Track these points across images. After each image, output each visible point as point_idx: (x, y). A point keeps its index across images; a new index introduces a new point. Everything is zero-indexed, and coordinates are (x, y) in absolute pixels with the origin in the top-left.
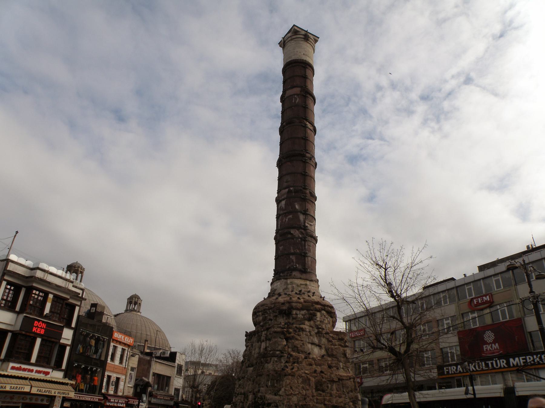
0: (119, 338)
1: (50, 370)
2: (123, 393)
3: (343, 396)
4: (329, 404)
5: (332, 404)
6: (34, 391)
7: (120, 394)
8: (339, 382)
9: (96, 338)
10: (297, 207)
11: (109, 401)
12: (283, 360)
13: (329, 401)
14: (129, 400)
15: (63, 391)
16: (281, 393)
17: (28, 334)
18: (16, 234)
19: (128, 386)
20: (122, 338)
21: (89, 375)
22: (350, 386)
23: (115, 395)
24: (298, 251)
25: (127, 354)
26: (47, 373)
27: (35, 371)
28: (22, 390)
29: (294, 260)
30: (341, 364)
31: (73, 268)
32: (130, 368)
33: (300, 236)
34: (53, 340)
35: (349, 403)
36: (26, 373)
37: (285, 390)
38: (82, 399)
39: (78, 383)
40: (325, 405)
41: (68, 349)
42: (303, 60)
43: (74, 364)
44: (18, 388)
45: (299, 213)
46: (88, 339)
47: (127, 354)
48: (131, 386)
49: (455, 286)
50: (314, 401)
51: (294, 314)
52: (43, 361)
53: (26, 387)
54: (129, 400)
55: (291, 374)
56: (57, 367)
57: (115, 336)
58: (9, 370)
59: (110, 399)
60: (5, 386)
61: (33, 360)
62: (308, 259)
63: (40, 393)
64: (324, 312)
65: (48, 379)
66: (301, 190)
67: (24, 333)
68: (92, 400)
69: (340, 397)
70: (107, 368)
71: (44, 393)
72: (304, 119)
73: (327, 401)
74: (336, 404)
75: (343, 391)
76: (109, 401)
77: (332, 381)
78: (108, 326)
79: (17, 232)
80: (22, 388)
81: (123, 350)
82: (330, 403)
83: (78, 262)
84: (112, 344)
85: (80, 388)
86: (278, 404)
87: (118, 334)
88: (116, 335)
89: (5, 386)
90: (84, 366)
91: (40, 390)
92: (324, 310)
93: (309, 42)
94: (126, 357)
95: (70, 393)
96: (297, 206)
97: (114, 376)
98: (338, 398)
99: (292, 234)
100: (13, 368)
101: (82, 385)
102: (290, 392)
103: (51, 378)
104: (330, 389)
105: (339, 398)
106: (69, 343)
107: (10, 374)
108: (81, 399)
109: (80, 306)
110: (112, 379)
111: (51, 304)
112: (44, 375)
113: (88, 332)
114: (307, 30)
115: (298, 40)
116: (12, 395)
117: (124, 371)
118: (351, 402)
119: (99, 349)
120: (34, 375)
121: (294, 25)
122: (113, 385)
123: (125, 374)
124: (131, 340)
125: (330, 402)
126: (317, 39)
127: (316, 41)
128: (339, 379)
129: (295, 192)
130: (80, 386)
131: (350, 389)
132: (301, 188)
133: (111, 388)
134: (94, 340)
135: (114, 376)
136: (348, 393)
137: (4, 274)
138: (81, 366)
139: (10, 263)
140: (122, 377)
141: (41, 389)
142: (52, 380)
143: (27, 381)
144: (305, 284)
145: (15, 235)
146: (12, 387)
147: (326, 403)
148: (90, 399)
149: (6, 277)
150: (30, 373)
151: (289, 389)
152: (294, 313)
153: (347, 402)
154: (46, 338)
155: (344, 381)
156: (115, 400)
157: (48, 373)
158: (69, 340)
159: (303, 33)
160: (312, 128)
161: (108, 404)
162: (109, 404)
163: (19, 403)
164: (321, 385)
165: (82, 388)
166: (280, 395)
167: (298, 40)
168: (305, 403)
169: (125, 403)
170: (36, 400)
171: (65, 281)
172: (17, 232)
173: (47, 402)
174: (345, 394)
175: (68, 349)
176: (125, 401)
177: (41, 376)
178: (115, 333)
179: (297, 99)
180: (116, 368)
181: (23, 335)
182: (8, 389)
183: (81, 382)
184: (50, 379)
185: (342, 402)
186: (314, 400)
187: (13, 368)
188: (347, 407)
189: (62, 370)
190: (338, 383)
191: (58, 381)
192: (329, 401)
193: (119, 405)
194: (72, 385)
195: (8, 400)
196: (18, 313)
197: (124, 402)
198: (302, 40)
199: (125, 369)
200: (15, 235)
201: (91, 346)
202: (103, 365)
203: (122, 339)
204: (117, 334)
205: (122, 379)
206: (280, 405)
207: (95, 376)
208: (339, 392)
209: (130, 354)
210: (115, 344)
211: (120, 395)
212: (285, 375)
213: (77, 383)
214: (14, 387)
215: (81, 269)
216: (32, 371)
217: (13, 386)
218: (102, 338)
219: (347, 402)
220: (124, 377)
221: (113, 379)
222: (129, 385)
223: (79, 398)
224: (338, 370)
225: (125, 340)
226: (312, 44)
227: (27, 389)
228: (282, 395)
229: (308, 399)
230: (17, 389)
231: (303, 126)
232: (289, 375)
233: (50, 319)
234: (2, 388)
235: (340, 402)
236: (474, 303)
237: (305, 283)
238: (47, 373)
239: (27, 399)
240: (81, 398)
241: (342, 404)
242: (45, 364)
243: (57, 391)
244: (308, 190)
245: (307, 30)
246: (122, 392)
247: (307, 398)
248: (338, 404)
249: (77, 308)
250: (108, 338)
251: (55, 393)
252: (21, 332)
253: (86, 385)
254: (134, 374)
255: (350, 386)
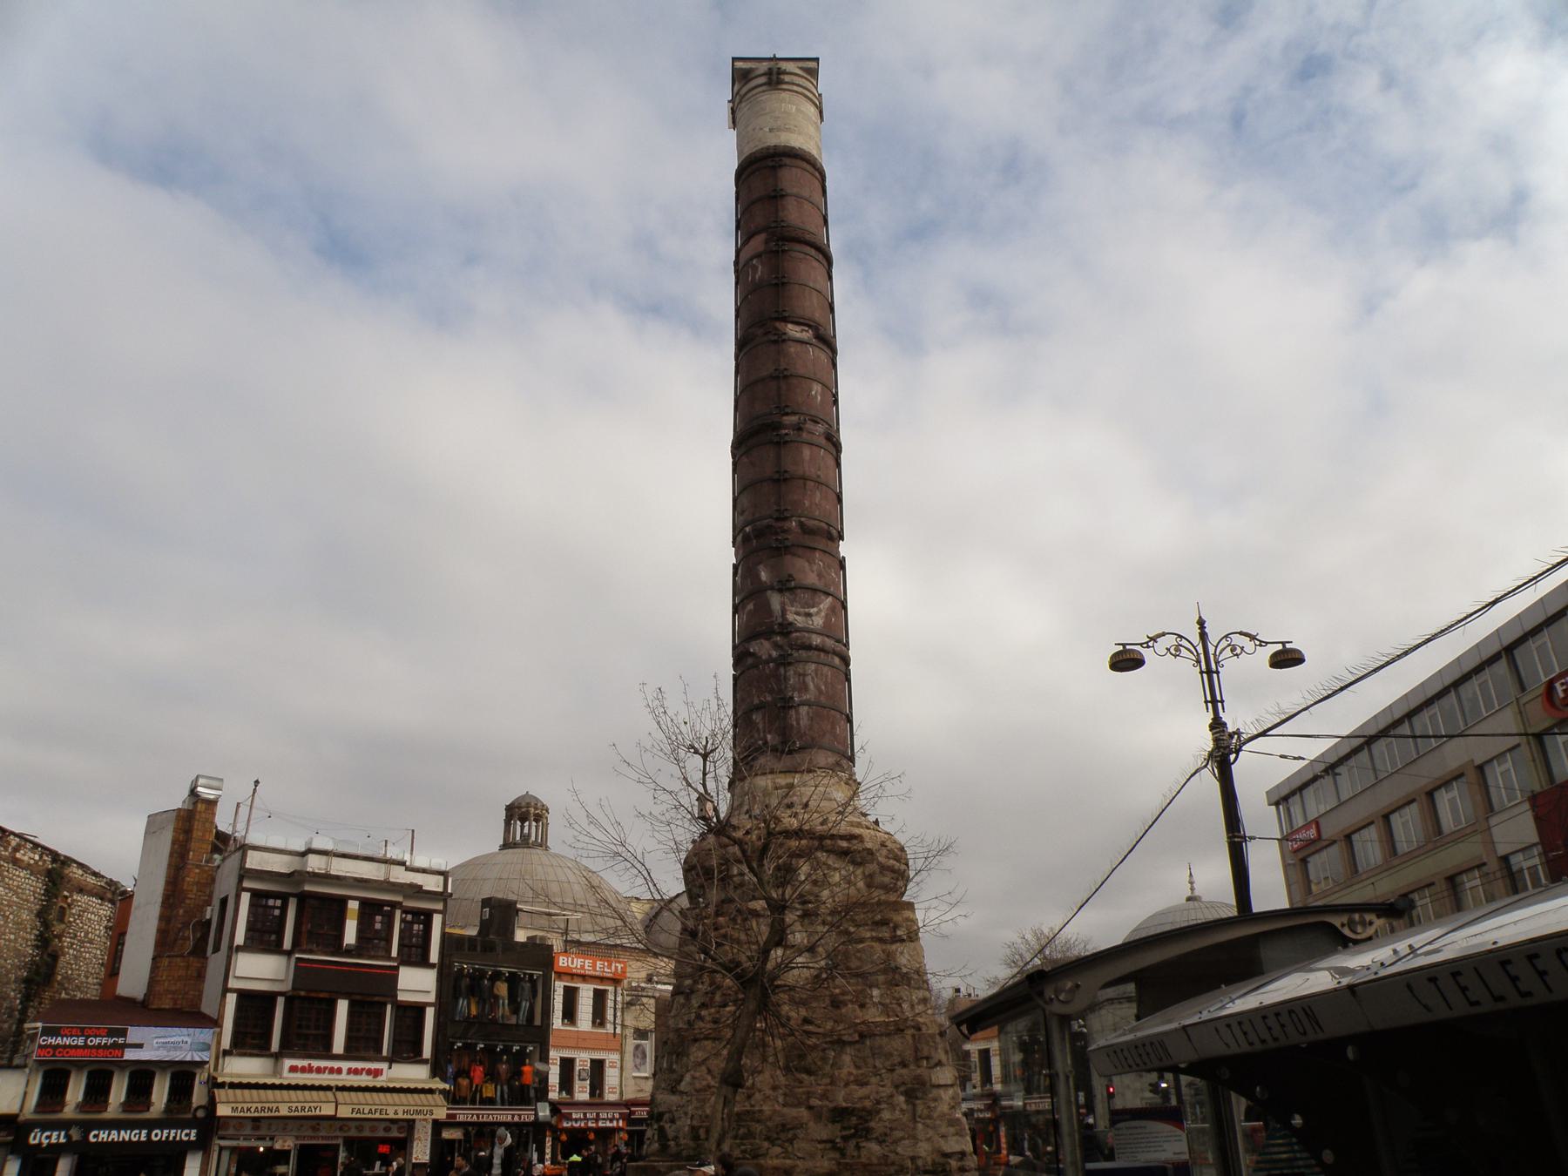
0: (576, 968)
1: (384, 1066)
2: (621, 1093)
3: (874, 1080)
4: (821, 1107)
5: (831, 1105)
6: (344, 1112)
7: (610, 1097)
8: (863, 1043)
9: (506, 977)
10: (764, 576)
11: (568, 1117)
12: (695, 1002)
13: (824, 1096)
14: (632, 1109)
15: (415, 1108)
16: (683, 1086)
17: (313, 995)
18: (256, 786)
19: (635, 1077)
20: (587, 964)
21: (503, 1063)
22: (897, 1050)
23: (597, 1100)
24: (769, 698)
25: (615, 1001)
26: (376, 1073)
27: (347, 1072)
28: (318, 1113)
29: (761, 726)
30: (876, 992)
31: (517, 810)
32: (629, 1032)
33: (774, 654)
34: (376, 999)
35: (892, 1096)
36: (326, 1076)
37: (694, 1078)
38: (488, 1120)
39: (477, 1086)
40: (810, 1108)
41: (430, 1013)
42: (768, 148)
43: (454, 1044)
44: (306, 1110)
45: (769, 592)
46: (486, 982)
47: (615, 1001)
48: (646, 1075)
49: (1500, 648)
50: (778, 1102)
51: (735, 876)
52: (363, 1044)
53: (324, 1106)
54: (632, 1109)
55: (711, 1036)
56: (414, 1056)
57: (561, 964)
58: (286, 1073)
59: (571, 1114)
60: (277, 1108)
61: (339, 1045)
62: (797, 713)
63: (358, 1116)
64: (822, 856)
65: (378, 1085)
66: (769, 526)
67: (303, 993)
68: (516, 1119)
69: (863, 1084)
70: (552, 1041)
71: (370, 1116)
72: (777, 319)
73: (817, 1098)
74: (844, 1105)
75: (875, 1067)
76: (568, 1117)
77: (841, 1043)
78: (539, 945)
79: (257, 782)
80: (315, 1109)
81: (599, 997)
82: (827, 1103)
83: (530, 793)
84: (559, 987)
85: (484, 1096)
86: (676, 1114)
87: (570, 959)
88: (563, 962)
89: (277, 1108)
90: (482, 1046)
91: (359, 1109)
92: (822, 848)
93: (784, 86)
94: (612, 1010)
95: (435, 1110)
96: (763, 573)
97: (583, 1059)
98: (853, 1087)
99: (753, 655)
100: (293, 1069)
101: (486, 1087)
102: (704, 1083)
103: (390, 1080)
104: (832, 1065)
105: (857, 1087)
106: (432, 998)
107: (285, 1083)
108: (485, 1120)
109: (443, 912)
110: (578, 1064)
111: (356, 922)
112: (370, 1078)
113: (477, 966)
114: (774, 55)
115: (753, 96)
116: (314, 1123)
117: (617, 1044)
118: (902, 1094)
119: (521, 1001)
120: (346, 1079)
121: (734, 59)
122: (584, 1080)
123: (617, 1050)
124: (616, 967)
125: (827, 1098)
126: (812, 65)
127: (813, 73)
128: (862, 1036)
129: (757, 537)
130: (484, 1090)
131: (897, 1060)
132: (770, 520)
133: (579, 1087)
134: (506, 981)
135: (583, 1059)
136: (892, 1071)
137: (241, 879)
138: (476, 1045)
139: (250, 853)
140: (611, 1058)
141: (361, 1107)
142: (388, 1087)
143: (329, 1094)
144: (787, 784)
145: (255, 790)
146: (293, 1109)
147: (815, 1102)
148: (509, 1119)
149: (246, 884)
150: (335, 1076)
151: (701, 1076)
152: (735, 872)
153: (884, 1095)
154: (358, 997)
155: (877, 1038)
156: (513, 1116)
157: (377, 1073)
158: (429, 992)
159: (764, 67)
160: (807, 335)
161: (565, 1125)
162: (569, 1125)
163: (336, 1137)
164: (802, 1057)
165: (490, 1095)
166: (682, 1093)
167: (753, 96)
168: (749, 1108)
169: (620, 1118)
170: (373, 1129)
171: (383, 865)
172: (257, 782)
173: (401, 1133)
174: (880, 1075)
175: (430, 1013)
176: (620, 1113)
177: (364, 1080)
178: (561, 958)
179: (757, 268)
180: (584, 1039)
181: (304, 998)
182: (284, 1112)
183: (486, 1082)
184: (385, 1085)
185: (868, 1097)
186: (777, 1097)
187: (293, 1069)
188: (883, 1109)
189: (425, 1062)
190: (857, 1046)
191: (420, 1086)
192: (824, 1096)
193: (604, 1125)
194: (443, 1092)
195: (310, 1133)
196: (289, 954)
197: (617, 1116)
198: (764, 91)
199: (615, 1037)
200: (255, 790)
201: (497, 997)
202: (540, 1036)
203: (586, 967)
204: (566, 959)
205: (580, 1061)
206: (680, 1118)
207: (525, 1065)
208: (860, 1072)
209: (623, 999)
210: (567, 982)
211: (610, 1099)
212: (696, 1040)
213: (474, 1086)
214: (297, 1107)
215: (536, 809)
216: (339, 1071)
217: (294, 1105)
218: (525, 974)
219: (881, 1098)
220: (615, 1057)
221: (580, 1065)
222: (635, 1074)
223: (478, 1117)
224: (864, 1010)
225: (598, 969)
226: (795, 88)
227: (328, 1110)
228: (686, 1091)
229: (758, 1096)
230: (272, 1112)
231: (775, 342)
232: (706, 1038)
233: (360, 956)
234: (272, 1112)
235: (861, 1098)
236: (1558, 696)
237: (789, 780)
238: (376, 1073)
239: (349, 1129)
240: (483, 1117)
241: (868, 1104)
242: (371, 1053)
243: (400, 1110)
244: (794, 518)
245: (774, 55)
246: (618, 1092)
247: (754, 1094)
248: (853, 1104)
249: (437, 920)
250: (541, 973)
251: (396, 1113)
252: (295, 993)
253: (499, 1088)
254: (649, 1045)
255: (897, 1050)
